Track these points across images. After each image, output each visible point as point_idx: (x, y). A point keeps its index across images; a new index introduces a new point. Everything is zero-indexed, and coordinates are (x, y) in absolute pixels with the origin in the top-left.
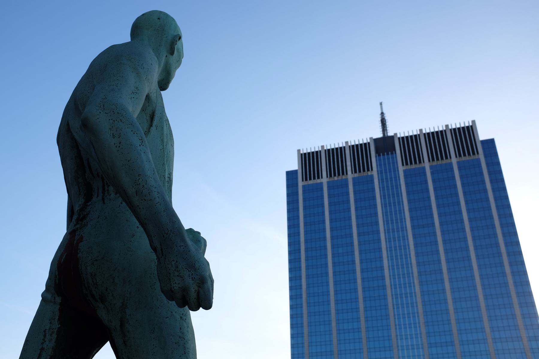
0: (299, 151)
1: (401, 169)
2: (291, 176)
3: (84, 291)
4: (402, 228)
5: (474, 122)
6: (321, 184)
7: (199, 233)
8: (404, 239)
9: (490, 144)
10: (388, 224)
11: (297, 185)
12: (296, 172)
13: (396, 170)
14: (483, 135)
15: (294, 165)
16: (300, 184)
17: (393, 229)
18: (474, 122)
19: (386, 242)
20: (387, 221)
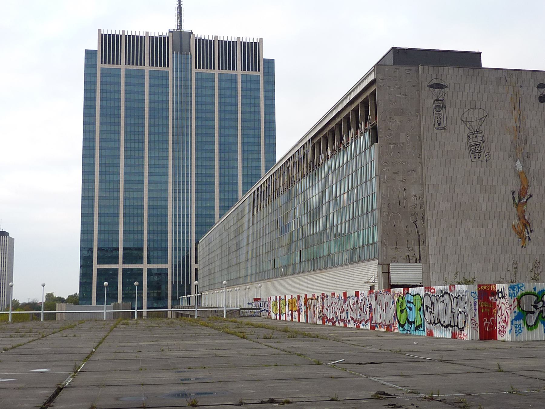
0: (100, 31)
1: (194, 71)
2: (90, 54)
3: (25, 405)
4: (188, 190)
5: (261, 40)
6: (120, 70)
7: (60, 297)
8: (188, 192)
9: (270, 63)
10: (176, 151)
11: (95, 66)
12: (95, 52)
13: (189, 71)
14: (266, 54)
15: (94, 45)
16: (99, 66)
17: (180, 88)
18: (261, 40)
19: (173, 176)
20: (176, 149)
